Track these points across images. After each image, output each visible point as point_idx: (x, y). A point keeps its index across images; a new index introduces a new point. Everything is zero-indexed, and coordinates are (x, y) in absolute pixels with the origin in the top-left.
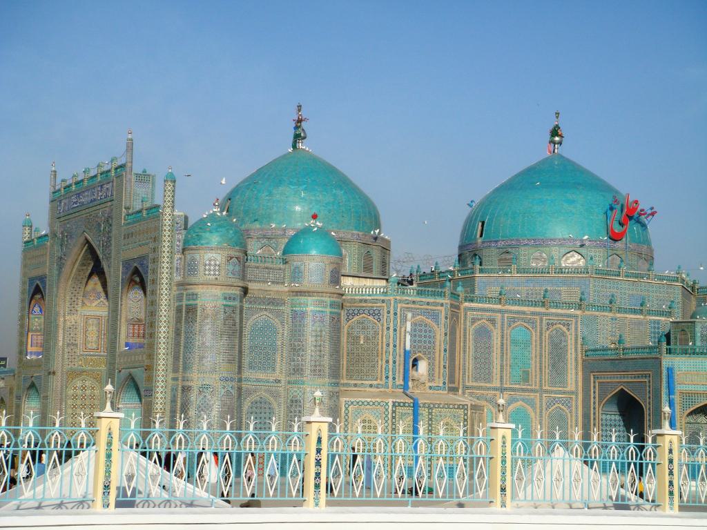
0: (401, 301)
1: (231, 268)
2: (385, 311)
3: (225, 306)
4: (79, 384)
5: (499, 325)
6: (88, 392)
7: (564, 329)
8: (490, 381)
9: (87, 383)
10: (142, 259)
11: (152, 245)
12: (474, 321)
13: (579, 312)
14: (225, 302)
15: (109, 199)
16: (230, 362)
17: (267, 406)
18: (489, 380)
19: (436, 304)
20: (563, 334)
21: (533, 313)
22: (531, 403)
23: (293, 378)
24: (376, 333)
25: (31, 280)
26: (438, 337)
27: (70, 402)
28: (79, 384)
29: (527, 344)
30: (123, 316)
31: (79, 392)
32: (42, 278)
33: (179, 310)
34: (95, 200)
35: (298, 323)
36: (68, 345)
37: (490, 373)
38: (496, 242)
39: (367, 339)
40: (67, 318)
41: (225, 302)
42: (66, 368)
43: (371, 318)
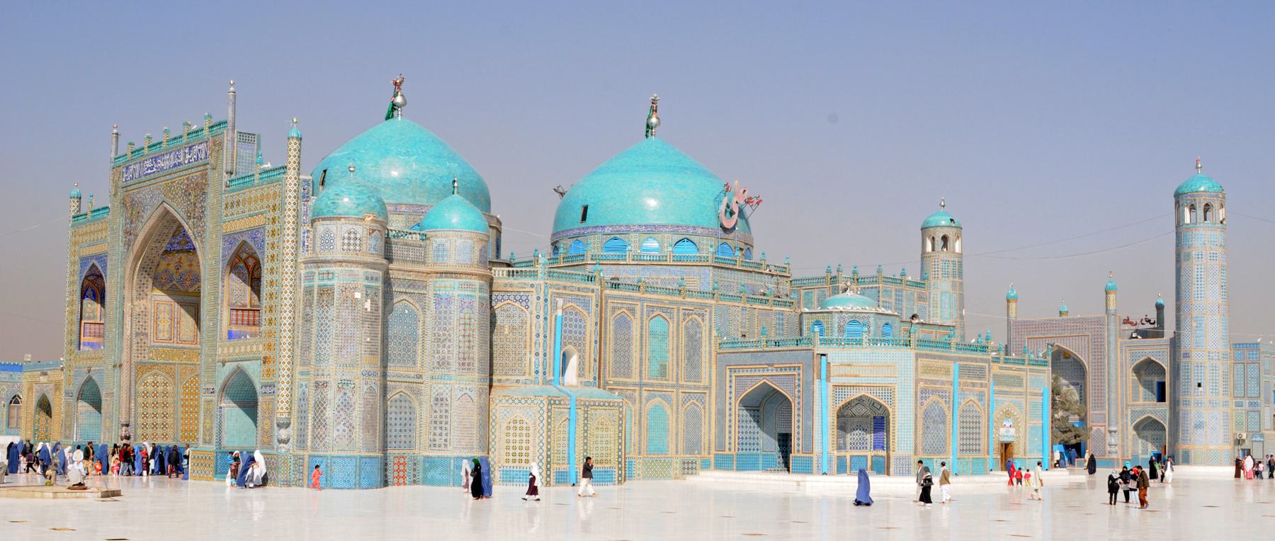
0: (552, 286)
1: (373, 242)
2: (535, 297)
3: (367, 287)
4: (150, 379)
5: (638, 315)
6: (160, 389)
7: (699, 319)
8: (628, 375)
9: (160, 379)
10: (255, 232)
11: (271, 215)
12: (614, 309)
13: (713, 302)
14: (366, 283)
15: (200, 162)
16: (372, 353)
18: (628, 375)
19: (587, 290)
20: (698, 326)
21: (671, 302)
22: (666, 398)
23: (438, 372)
24: (524, 322)
25: (84, 260)
27: (140, 400)
28: (150, 379)
29: (664, 336)
30: (226, 299)
31: (150, 389)
32: (102, 258)
33: (309, 291)
34: (180, 164)
35: (443, 310)
36: (137, 334)
37: (629, 367)
38: (603, 227)
39: (513, 329)
40: (136, 303)
41: (366, 283)
42: (134, 360)
43: (517, 304)
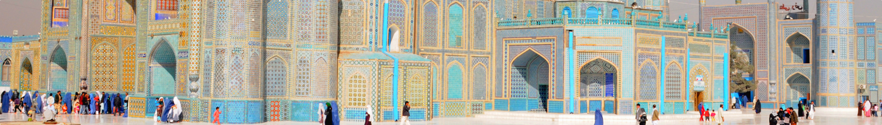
6: (108, 54)
7: (484, 6)
8: (435, 45)
9: (108, 47)
16: (256, 30)
17: (280, 65)
18: (435, 45)
20: (483, 10)
22: (462, 61)
23: (302, 43)
24: (361, 8)
26: (407, 11)
27: (94, 62)
28: (101, 48)
29: (460, 17)
31: (101, 54)
36: (92, 16)
37: (435, 39)
39: (354, 12)
42: (90, 34)
